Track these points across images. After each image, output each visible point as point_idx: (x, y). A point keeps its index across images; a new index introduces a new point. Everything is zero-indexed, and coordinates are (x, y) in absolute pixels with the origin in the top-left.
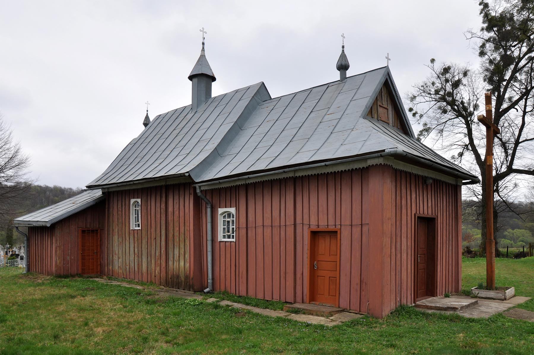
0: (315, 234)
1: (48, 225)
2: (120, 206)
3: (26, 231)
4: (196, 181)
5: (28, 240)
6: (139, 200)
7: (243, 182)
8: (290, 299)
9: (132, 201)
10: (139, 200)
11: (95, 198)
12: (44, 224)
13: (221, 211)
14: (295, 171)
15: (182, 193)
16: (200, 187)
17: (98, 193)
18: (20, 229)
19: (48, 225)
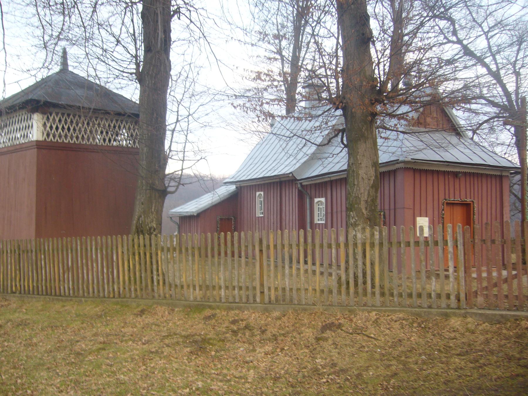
0: (467, 206)
1: (195, 215)
2: (457, 186)
3: (177, 220)
4: (298, 178)
5: (179, 228)
6: (262, 193)
7: (329, 179)
8: (237, 300)
9: (258, 193)
10: (262, 193)
11: (230, 192)
12: (192, 214)
13: (316, 200)
14: (501, 171)
15: (480, 179)
16: (301, 184)
17: (233, 188)
18: (174, 219)
19: (195, 215)
